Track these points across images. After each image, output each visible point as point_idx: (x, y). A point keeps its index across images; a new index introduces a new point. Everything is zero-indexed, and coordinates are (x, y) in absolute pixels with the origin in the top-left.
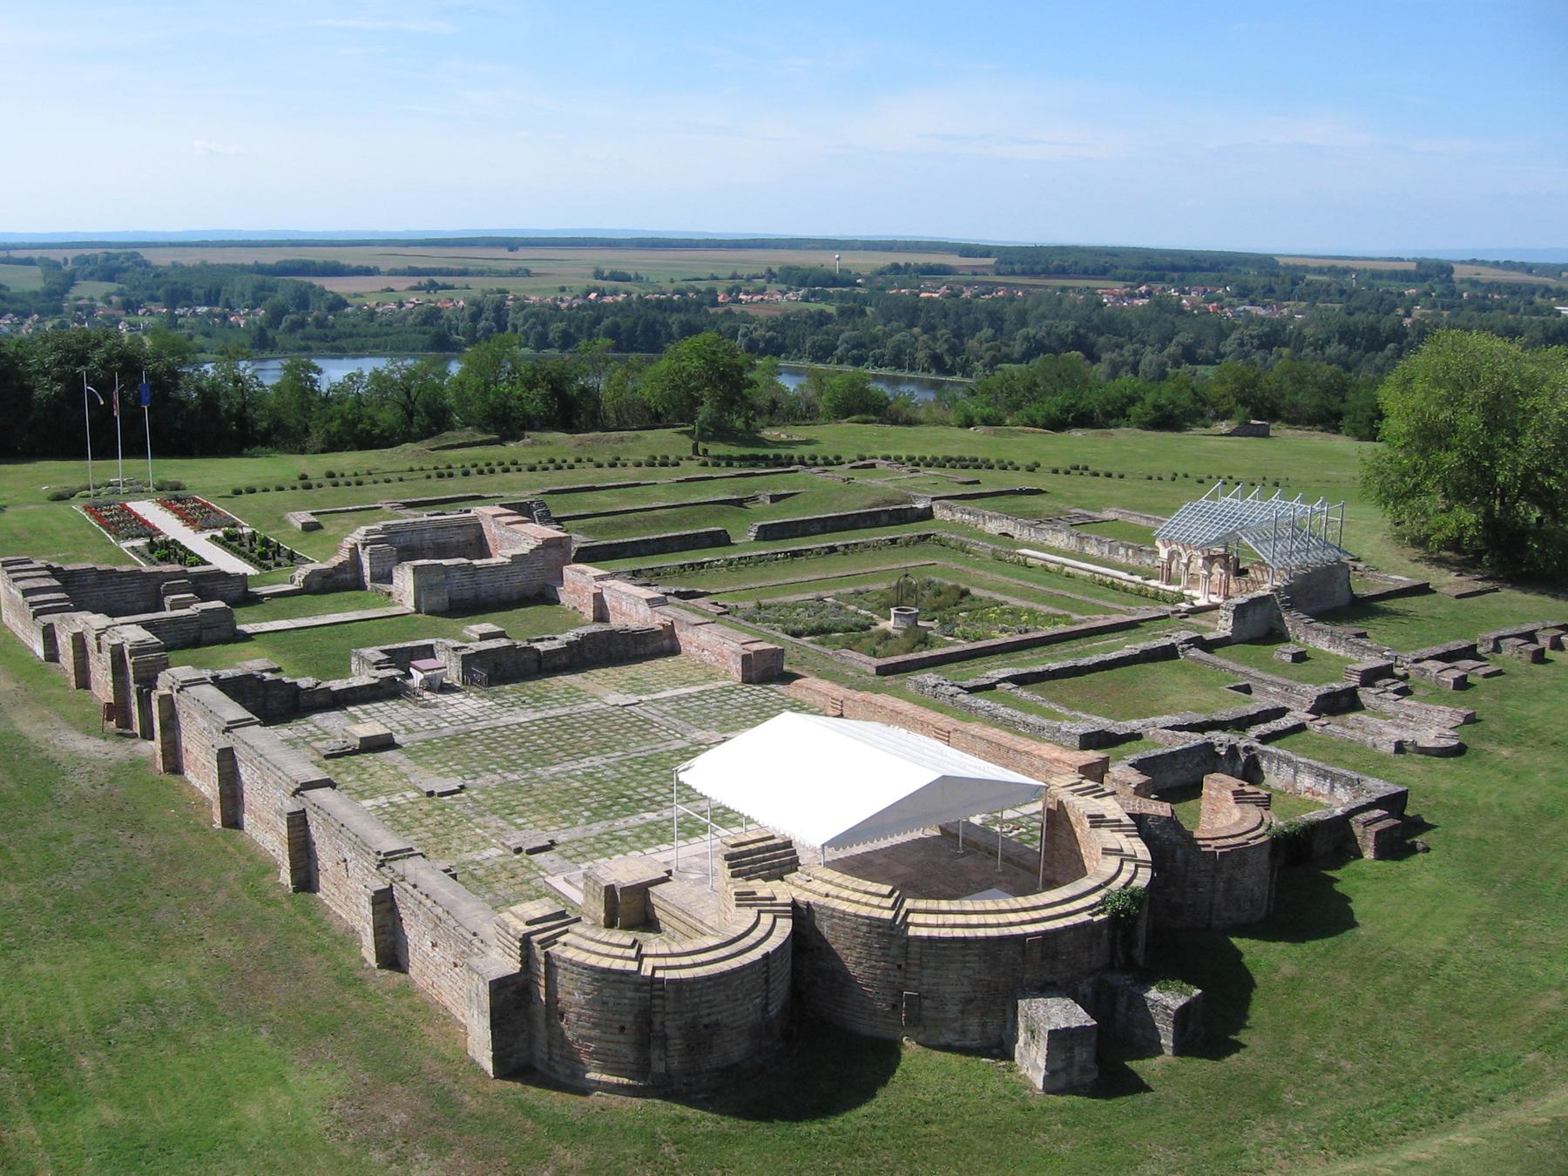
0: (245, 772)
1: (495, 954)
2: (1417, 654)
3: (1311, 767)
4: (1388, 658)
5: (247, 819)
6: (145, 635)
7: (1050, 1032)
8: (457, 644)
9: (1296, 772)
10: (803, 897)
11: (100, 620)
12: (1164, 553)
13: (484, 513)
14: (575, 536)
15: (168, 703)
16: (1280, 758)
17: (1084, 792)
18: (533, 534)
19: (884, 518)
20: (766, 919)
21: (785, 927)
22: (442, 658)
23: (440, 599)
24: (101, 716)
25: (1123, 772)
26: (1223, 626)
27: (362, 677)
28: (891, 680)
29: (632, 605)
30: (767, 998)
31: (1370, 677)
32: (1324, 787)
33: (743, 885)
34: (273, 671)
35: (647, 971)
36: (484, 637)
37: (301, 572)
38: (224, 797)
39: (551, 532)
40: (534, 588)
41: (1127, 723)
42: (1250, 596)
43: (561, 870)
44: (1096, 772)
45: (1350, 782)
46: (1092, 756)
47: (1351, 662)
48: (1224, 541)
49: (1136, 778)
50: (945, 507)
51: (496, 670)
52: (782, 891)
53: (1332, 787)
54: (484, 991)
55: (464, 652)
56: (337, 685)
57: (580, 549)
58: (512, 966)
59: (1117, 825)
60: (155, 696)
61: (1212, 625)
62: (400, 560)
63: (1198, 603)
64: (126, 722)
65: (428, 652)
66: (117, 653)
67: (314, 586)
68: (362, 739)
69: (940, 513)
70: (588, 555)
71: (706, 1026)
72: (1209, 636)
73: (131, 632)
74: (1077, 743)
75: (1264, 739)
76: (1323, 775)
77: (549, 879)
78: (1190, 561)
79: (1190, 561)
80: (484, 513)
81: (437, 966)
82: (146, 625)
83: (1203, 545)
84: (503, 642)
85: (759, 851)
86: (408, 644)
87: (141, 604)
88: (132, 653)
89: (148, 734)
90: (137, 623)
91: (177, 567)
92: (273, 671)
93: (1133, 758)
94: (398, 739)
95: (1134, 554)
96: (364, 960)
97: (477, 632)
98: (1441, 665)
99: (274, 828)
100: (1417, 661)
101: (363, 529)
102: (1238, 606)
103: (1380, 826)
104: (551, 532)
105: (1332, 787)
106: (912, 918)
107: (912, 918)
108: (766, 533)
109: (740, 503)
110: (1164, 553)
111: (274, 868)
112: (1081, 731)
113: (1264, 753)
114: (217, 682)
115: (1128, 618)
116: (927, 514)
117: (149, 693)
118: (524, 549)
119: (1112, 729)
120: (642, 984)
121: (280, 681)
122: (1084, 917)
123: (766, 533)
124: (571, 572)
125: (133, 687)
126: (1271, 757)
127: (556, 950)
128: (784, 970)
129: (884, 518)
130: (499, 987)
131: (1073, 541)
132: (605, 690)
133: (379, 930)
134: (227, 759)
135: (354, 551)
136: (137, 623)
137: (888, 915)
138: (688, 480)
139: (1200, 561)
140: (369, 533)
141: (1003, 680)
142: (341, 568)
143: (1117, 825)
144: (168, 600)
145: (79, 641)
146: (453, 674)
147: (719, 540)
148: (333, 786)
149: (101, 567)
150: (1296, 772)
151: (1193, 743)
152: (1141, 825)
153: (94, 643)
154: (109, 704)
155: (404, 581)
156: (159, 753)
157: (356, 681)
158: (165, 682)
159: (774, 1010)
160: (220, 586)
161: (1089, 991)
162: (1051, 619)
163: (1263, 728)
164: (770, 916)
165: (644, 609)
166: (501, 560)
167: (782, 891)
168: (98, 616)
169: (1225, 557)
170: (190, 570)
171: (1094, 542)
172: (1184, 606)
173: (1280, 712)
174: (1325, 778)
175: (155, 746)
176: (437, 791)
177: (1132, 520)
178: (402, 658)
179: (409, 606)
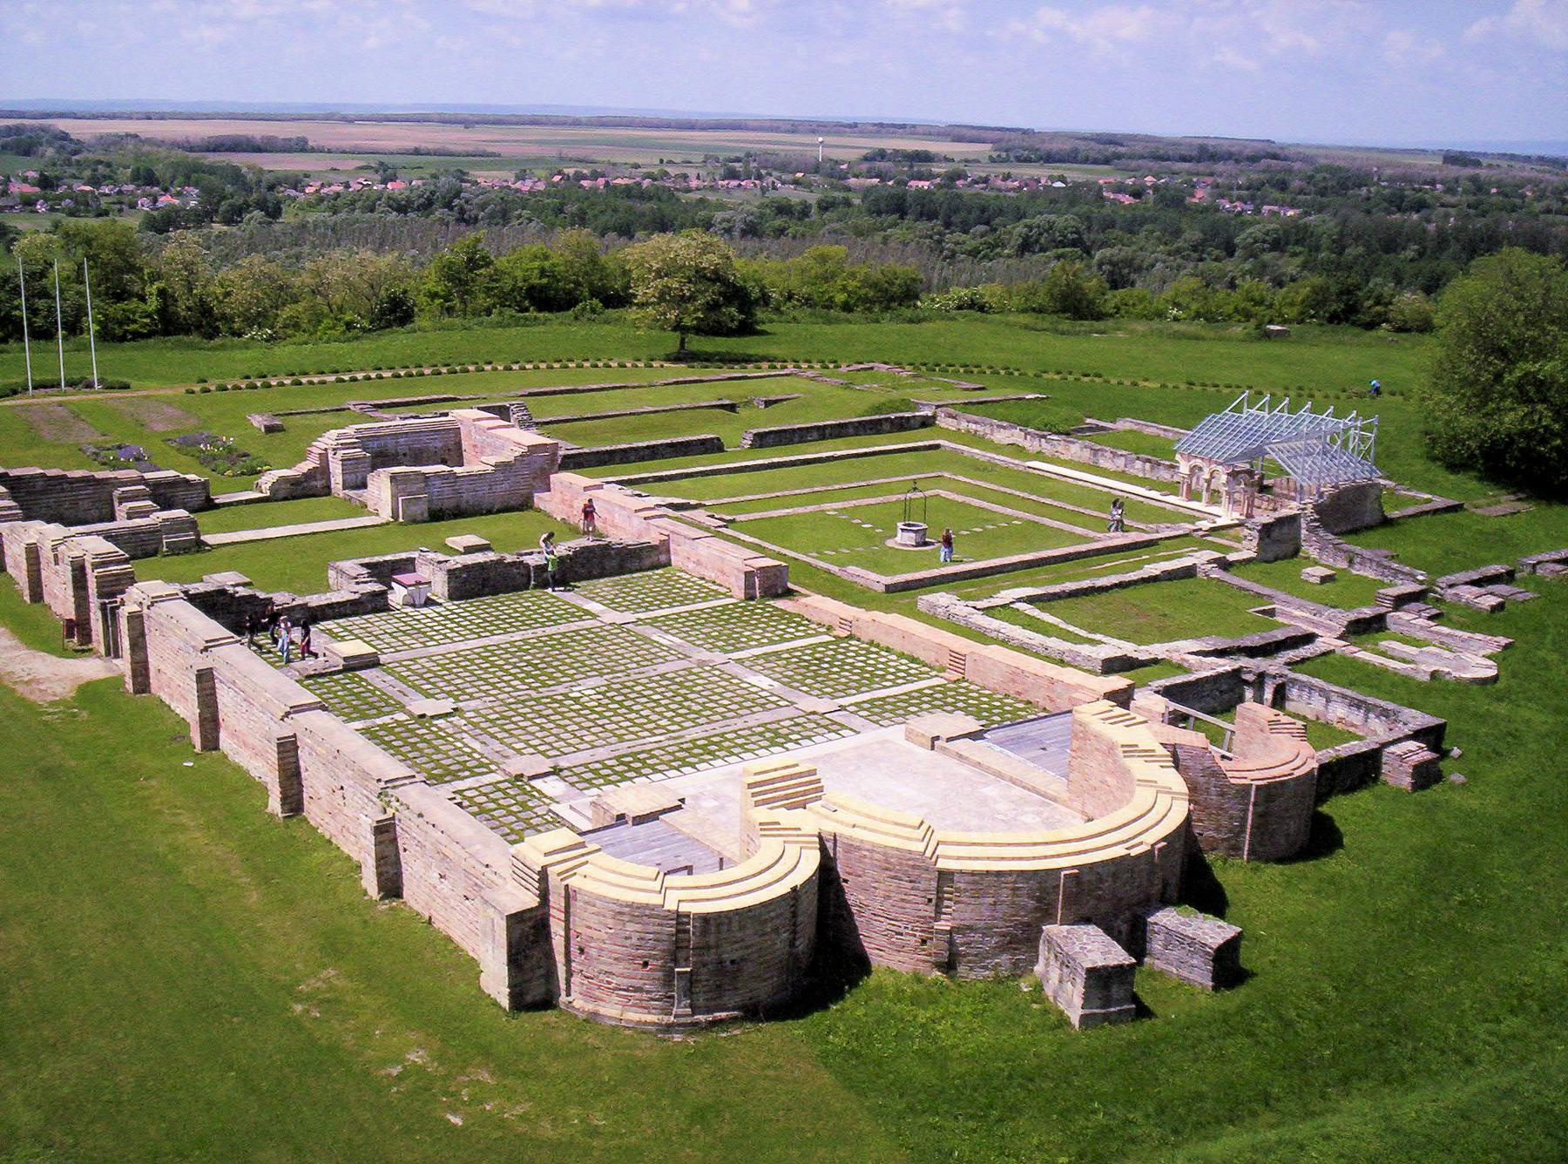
0: (224, 697)
1: (512, 886)
2: (1452, 578)
3: (1344, 697)
4: (1421, 583)
5: (223, 736)
6: (110, 547)
7: (1090, 971)
8: (441, 557)
9: (1328, 701)
10: (829, 827)
11: (55, 530)
12: (1184, 468)
13: (464, 416)
14: (561, 443)
15: (136, 619)
16: (1311, 688)
17: (1114, 721)
18: (516, 439)
19: (886, 426)
20: (792, 850)
21: (810, 864)
22: (423, 572)
23: (421, 509)
24: (62, 632)
25: (1149, 701)
26: (1247, 550)
27: (343, 593)
28: (903, 598)
29: (624, 513)
30: (794, 932)
31: (1401, 601)
32: (1356, 717)
33: (763, 814)
34: (244, 585)
35: (671, 905)
36: (470, 550)
37: (268, 480)
38: (203, 721)
39: (532, 438)
40: (512, 495)
41: (1150, 648)
42: (1277, 515)
43: (567, 797)
44: (1122, 698)
45: (1385, 713)
46: (1118, 682)
47: (1383, 585)
48: (1249, 455)
49: (1161, 704)
50: (950, 416)
51: (472, 584)
52: (810, 821)
53: (1366, 718)
54: (502, 924)
55: (448, 566)
56: (315, 600)
57: (565, 457)
58: (531, 901)
59: (1148, 754)
60: (124, 612)
61: (1236, 545)
62: (374, 468)
63: (1220, 522)
64: (86, 637)
65: (408, 565)
66: (79, 572)
67: (282, 494)
68: (345, 659)
69: (943, 422)
70: (574, 463)
71: (733, 962)
72: (1232, 557)
73: (91, 544)
74: (1099, 669)
75: (1291, 664)
76: (1357, 704)
77: (554, 807)
78: (1212, 477)
79: (1212, 477)
80: (464, 416)
81: (445, 899)
82: (109, 536)
83: (1226, 460)
84: (491, 556)
85: (783, 779)
86: (388, 558)
87: (95, 513)
88: (95, 566)
89: (113, 651)
90: (98, 533)
91: (134, 474)
92: (244, 585)
93: (1156, 684)
94: (383, 659)
95: (1152, 468)
96: (365, 893)
97: (465, 542)
98: (1475, 589)
99: (234, 734)
100: (1451, 586)
101: (334, 433)
102: (1264, 525)
103: (1416, 759)
104: (532, 438)
105: (1366, 718)
106: (941, 850)
107: (941, 850)
108: (762, 441)
109: (732, 408)
110: (1184, 468)
111: (264, 790)
112: (1103, 656)
113: (1294, 681)
114: (193, 599)
115: (1146, 537)
116: (927, 423)
117: (114, 610)
118: (508, 456)
119: (1135, 655)
120: (665, 917)
121: (254, 597)
122: (1120, 851)
123: (762, 441)
124: (560, 479)
125: (94, 603)
126: (1303, 686)
127: (574, 882)
128: (809, 905)
129: (886, 426)
130: (515, 920)
131: (1087, 454)
132: (594, 603)
133: (381, 860)
134: (206, 680)
135: (324, 457)
136: (98, 533)
137: (920, 847)
138: (677, 383)
139: (1224, 478)
140: (339, 437)
141: (1019, 600)
142: (309, 476)
143: (1148, 754)
144: (121, 510)
145: (33, 553)
146: (440, 588)
147: (712, 446)
148: (324, 709)
149: (51, 472)
150: (1328, 701)
151: (1221, 670)
152: (1176, 758)
153: (51, 555)
154: (70, 621)
155: (380, 490)
156: (129, 673)
157: (335, 598)
158: (133, 598)
159: (802, 944)
160: (180, 493)
161: (1124, 928)
162: (1029, 534)
163: (1291, 654)
164: (797, 847)
165: (637, 521)
166: (482, 467)
167: (810, 821)
168: (52, 526)
169: (1250, 473)
170: (148, 475)
171: (1108, 454)
172: (1205, 525)
173: (1309, 638)
174: (1359, 708)
175: (124, 665)
176: (631, 814)
177: (1148, 431)
178: (384, 572)
179: (386, 515)
